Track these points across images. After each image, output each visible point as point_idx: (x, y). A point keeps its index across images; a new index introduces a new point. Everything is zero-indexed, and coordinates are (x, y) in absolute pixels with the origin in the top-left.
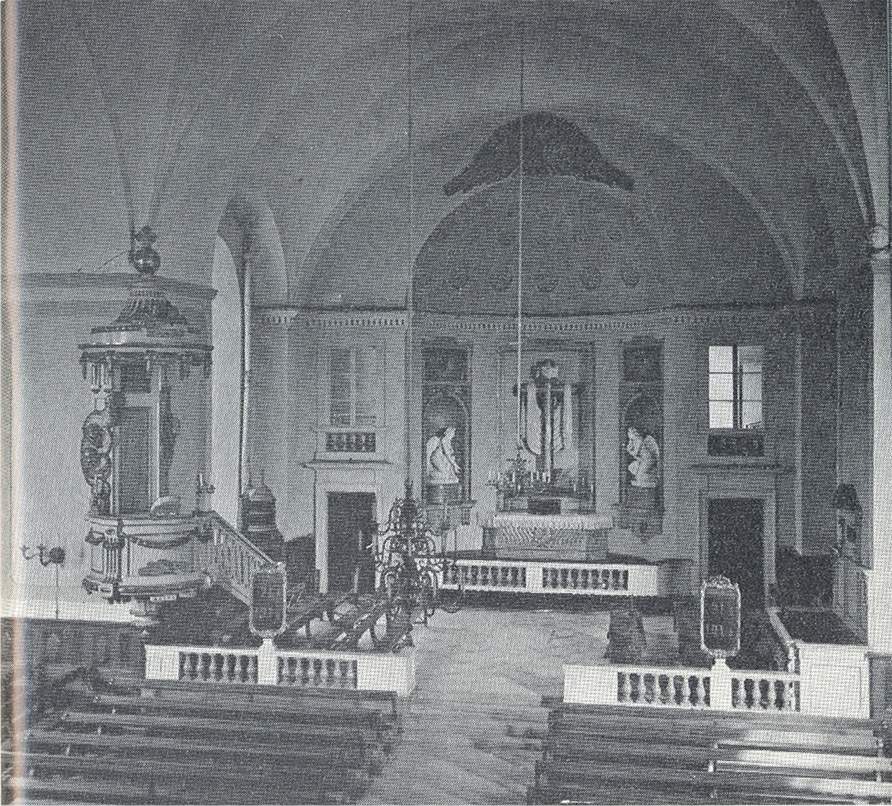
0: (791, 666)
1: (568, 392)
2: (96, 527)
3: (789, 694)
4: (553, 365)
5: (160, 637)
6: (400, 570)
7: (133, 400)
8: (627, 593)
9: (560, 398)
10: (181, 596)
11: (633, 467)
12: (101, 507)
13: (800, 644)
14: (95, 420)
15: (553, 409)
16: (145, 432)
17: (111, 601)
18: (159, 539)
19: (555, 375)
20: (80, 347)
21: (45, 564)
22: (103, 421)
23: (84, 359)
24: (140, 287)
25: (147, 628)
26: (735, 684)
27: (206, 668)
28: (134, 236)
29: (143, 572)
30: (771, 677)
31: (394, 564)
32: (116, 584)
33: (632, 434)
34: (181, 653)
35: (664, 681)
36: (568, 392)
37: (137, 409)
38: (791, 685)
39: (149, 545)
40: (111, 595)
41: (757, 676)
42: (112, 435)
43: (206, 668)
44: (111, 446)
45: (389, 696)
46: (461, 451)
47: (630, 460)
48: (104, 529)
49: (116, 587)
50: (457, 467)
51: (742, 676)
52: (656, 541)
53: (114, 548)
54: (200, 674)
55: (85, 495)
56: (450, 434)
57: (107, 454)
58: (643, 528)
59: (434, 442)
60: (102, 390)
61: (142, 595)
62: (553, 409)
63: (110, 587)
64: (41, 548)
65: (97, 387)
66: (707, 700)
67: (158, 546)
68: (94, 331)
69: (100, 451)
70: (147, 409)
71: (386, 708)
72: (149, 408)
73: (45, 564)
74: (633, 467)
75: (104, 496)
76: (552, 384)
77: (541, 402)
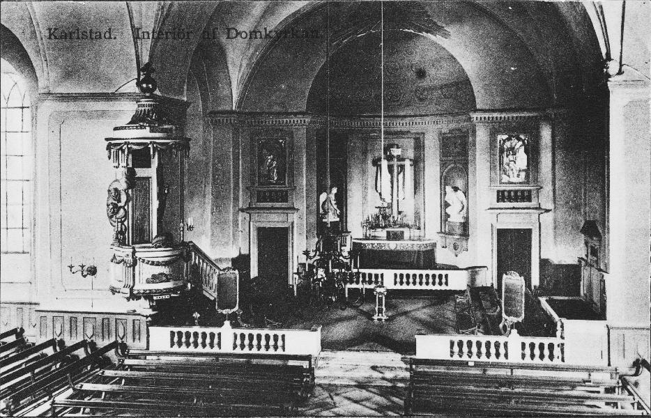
0: (558, 334)
1: (407, 163)
2: (117, 253)
3: (557, 351)
4: (398, 148)
5: (156, 321)
6: (322, 280)
7: (141, 173)
8: (448, 288)
9: (402, 168)
10: (172, 295)
11: (448, 210)
12: (121, 240)
13: (564, 320)
14: (116, 185)
15: (398, 174)
16: (147, 191)
17: (128, 299)
18: (161, 260)
19: (400, 154)
20: (107, 139)
21: (85, 276)
22: (122, 185)
23: (109, 148)
24: (143, 102)
25: (150, 316)
26: (523, 345)
27: (268, 343)
28: (139, 70)
29: (148, 282)
30: (546, 341)
31: (319, 277)
32: (131, 290)
33: (449, 189)
34: (171, 332)
35: (188, 335)
36: (407, 163)
37: (144, 178)
38: (558, 346)
39: (153, 263)
40: (128, 295)
41: (537, 341)
42: (127, 194)
43: (268, 343)
44: (127, 202)
45: (308, 358)
46: (342, 200)
47: (447, 205)
48: (123, 255)
49: (131, 290)
50: (338, 211)
51: (528, 340)
52: (463, 255)
53: (130, 267)
54: (192, 345)
55: (110, 232)
56: (335, 190)
57: (123, 207)
58: (455, 248)
59: (323, 197)
60: (120, 166)
61: (148, 296)
62: (398, 174)
63: (128, 290)
64: (83, 267)
65: (117, 165)
66: (506, 356)
67: (158, 264)
68: (116, 129)
69: (119, 205)
70: (148, 179)
71: (305, 364)
72: (151, 177)
73: (85, 276)
74: (448, 210)
75: (121, 232)
76: (397, 158)
77: (390, 169)
